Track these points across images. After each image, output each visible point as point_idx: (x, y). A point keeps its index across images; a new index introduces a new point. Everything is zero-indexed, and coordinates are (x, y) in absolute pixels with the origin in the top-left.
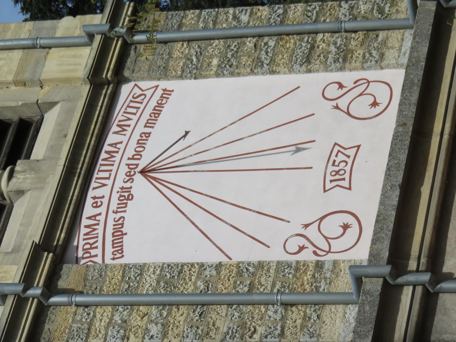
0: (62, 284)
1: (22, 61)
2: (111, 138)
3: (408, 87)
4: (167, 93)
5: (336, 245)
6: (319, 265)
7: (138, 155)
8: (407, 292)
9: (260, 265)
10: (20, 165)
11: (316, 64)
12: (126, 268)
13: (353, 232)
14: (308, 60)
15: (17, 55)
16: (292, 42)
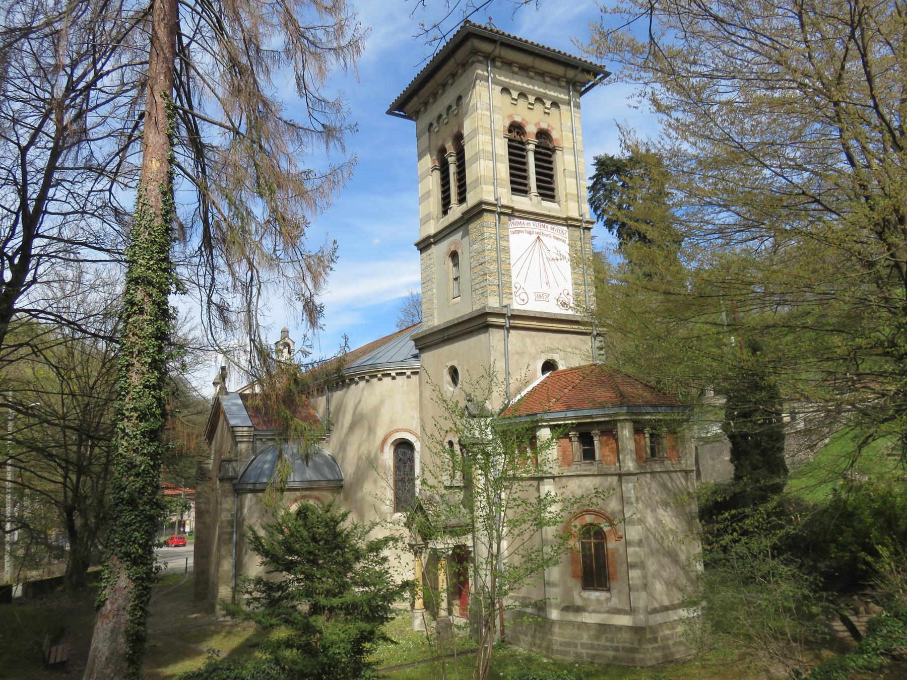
0: (502, 217)
1: (573, 195)
2: (549, 226)
3: (479, 463)
4: (564, 241)
5: (518, 298)
6: (511, 294)
7: (544, 234)
8: (503, 320)
9: (510, 276)
10: (540, 198)
11: (575, 286)
12: (508, 236)
13: (522, 303)
14: (576, 284)
15: (576, 193)
16: (581, 278)
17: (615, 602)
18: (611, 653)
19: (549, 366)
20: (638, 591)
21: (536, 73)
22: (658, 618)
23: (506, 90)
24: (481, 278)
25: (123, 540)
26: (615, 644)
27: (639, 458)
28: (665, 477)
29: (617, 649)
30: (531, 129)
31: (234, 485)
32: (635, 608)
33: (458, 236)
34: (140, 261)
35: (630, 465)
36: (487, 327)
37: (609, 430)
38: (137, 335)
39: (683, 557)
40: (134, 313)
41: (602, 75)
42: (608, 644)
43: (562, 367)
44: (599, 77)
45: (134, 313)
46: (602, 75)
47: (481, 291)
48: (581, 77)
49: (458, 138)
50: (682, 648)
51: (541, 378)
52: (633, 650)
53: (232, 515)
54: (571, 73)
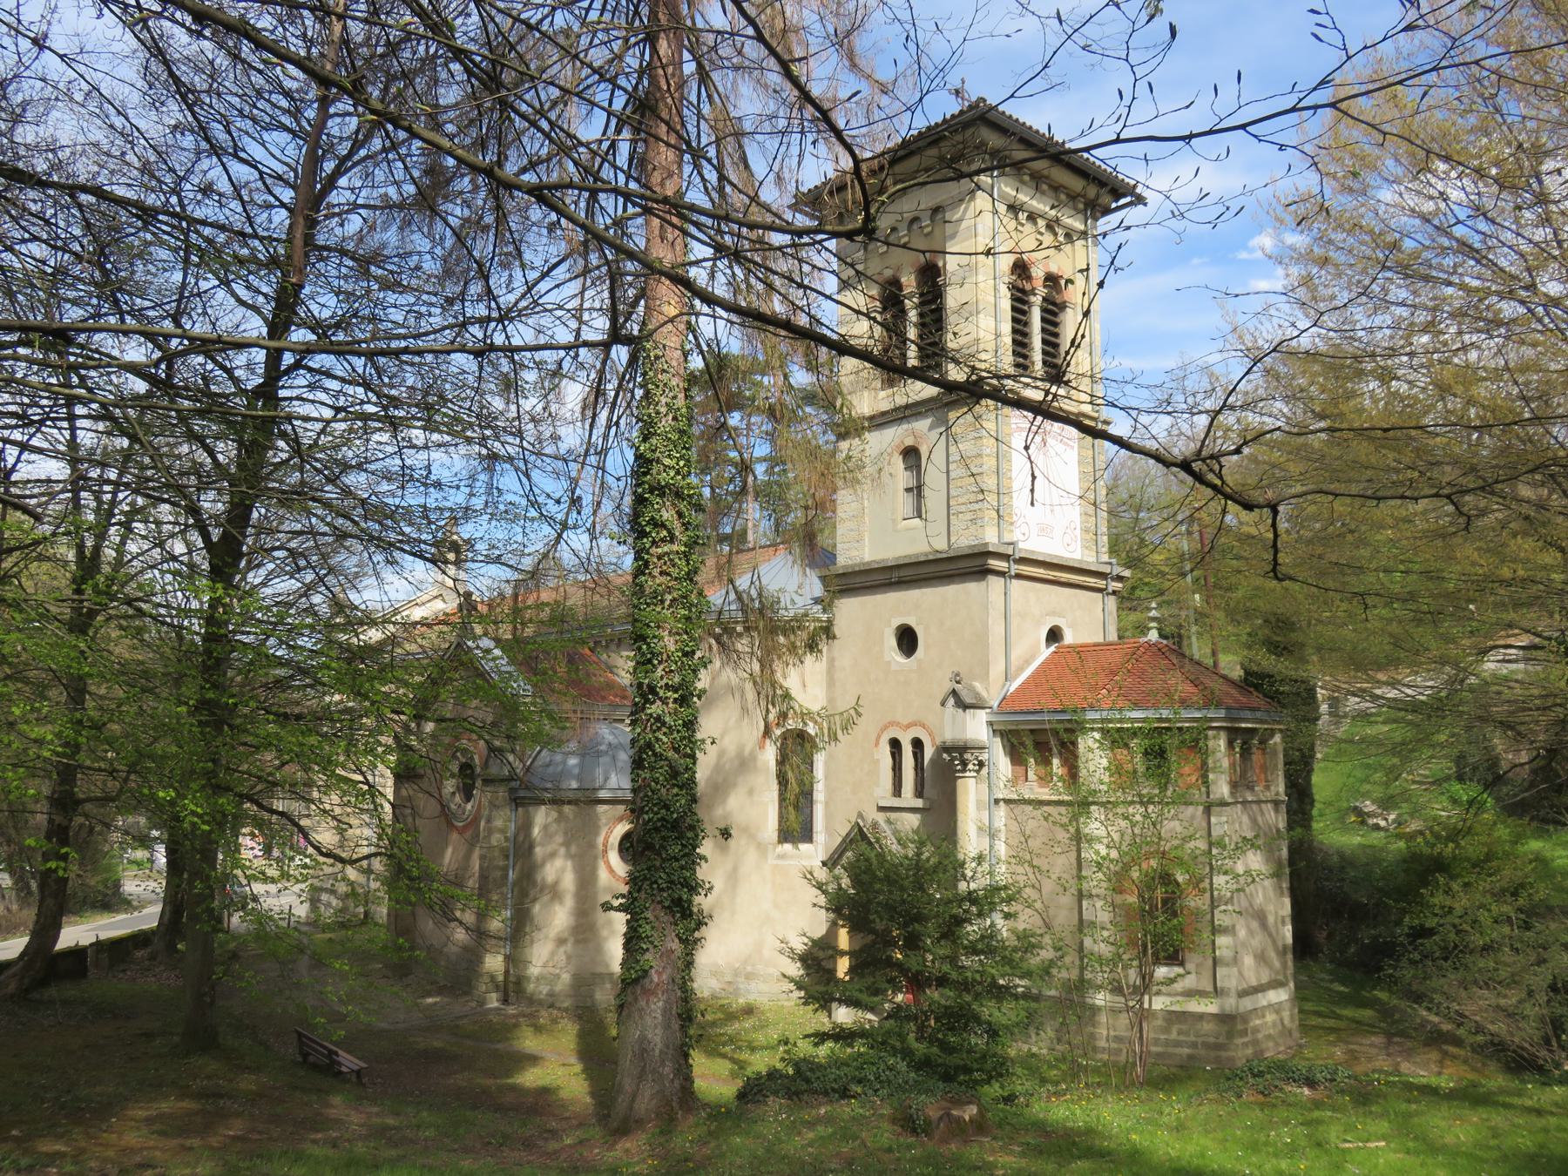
8: (1005, 564)
17: (1189, 982)
18: (1186, 1051)
19: (1054, 635)
20: (1227, 965)
21: (1051, 186)
22: (1247, 1004)
23: (1014, 208)
24: (972, 497)
25: (672, 882)
26: (1193, 1038)
27: (1234, 785)
28: (1255, 807)
29: (1194, 1045)
30: (1038, 273)
31: (512, 791)
32: (1222, 990)
33: (923, 424)
34: (667, 461)
35: (1222, 789)
36: (984, 573)
37: (1195, 743)
38: (668, 574)
39: (1271, 919)
40: (663, 540)
41: (1128, 199)
42: (1182, 1038)
43: (1069, 638)
44: (1123, 201)
45: (663, 540)
46: (1128, 199)
47: (969, 516)
48: (1105, 199)
49: (931, 277)
50: (1271, 1044)
51: (1046, 652)
52: (1218, 1047)
53: (507, 839)
54: (1092, 191)
